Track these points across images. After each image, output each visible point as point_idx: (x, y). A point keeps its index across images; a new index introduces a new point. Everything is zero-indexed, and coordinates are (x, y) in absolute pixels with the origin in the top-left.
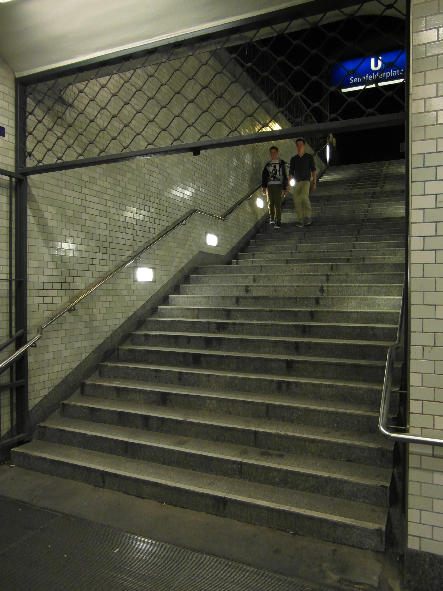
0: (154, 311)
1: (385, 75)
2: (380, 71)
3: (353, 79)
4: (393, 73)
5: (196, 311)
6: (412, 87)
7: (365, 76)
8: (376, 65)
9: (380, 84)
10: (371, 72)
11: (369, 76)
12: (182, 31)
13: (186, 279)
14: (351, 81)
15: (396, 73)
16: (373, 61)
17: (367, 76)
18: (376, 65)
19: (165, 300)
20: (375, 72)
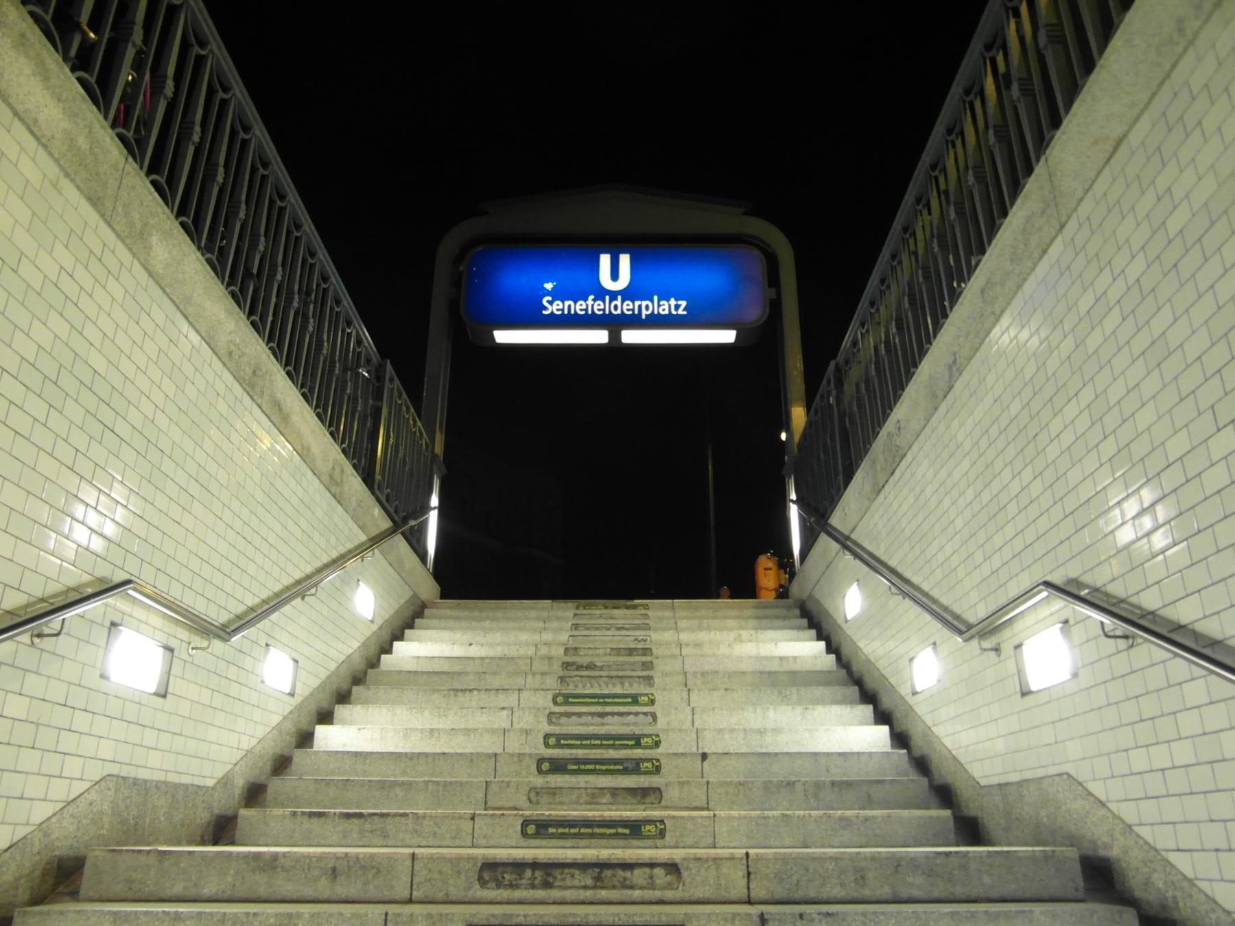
0: (305, 739)
1: (640, 307)
2: (627, 294)
3: (551, 303)
4: (659, 306)
5: (430, 786)
6: (473, 846)
7: (586, 300)
8: (615, 276)
9: (630, 337)
10: (601, 293)
11: (594, 300)
12: (226, 68)
13: (343, 697)
14: (546, 308)
15: (666, 307)
16: (605, 260)
17: (590, 302)
18: (615, 276)
19: (388, 650)
20: (613, 295)
